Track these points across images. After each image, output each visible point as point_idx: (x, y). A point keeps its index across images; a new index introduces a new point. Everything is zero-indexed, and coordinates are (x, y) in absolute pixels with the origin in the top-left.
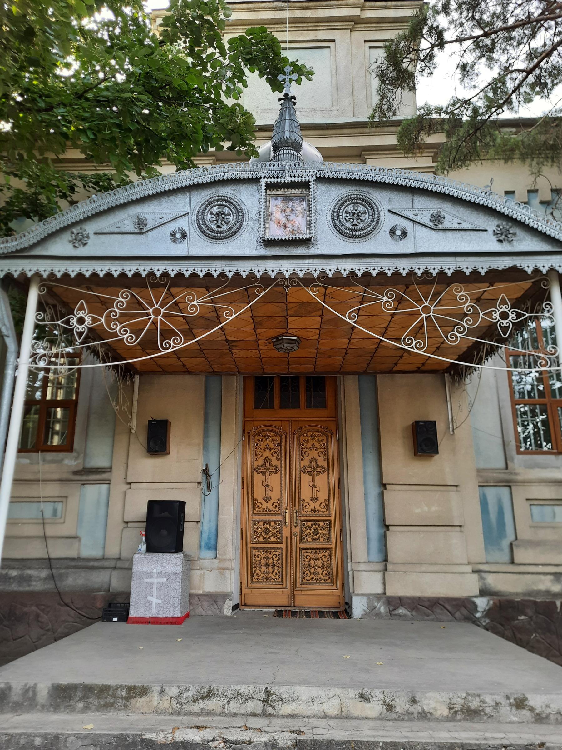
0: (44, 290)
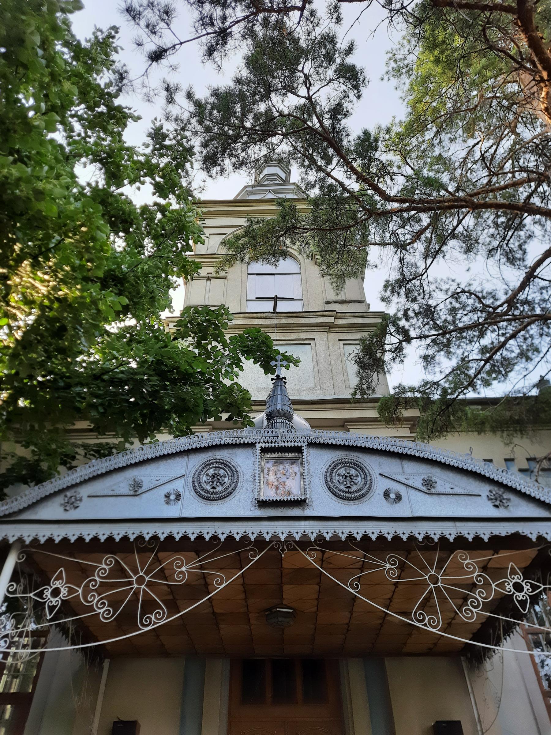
0: (23, 557)
